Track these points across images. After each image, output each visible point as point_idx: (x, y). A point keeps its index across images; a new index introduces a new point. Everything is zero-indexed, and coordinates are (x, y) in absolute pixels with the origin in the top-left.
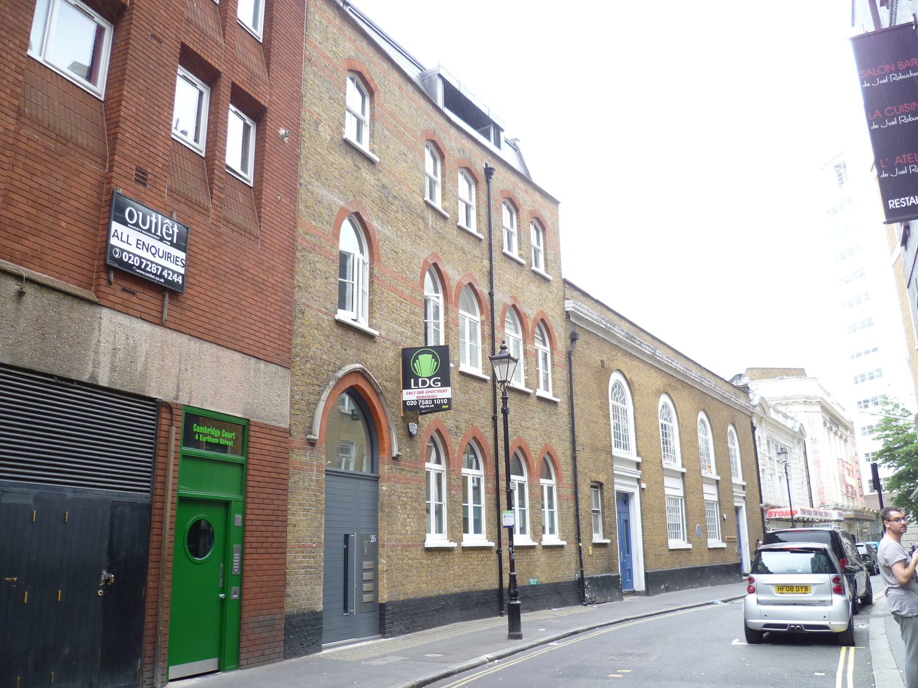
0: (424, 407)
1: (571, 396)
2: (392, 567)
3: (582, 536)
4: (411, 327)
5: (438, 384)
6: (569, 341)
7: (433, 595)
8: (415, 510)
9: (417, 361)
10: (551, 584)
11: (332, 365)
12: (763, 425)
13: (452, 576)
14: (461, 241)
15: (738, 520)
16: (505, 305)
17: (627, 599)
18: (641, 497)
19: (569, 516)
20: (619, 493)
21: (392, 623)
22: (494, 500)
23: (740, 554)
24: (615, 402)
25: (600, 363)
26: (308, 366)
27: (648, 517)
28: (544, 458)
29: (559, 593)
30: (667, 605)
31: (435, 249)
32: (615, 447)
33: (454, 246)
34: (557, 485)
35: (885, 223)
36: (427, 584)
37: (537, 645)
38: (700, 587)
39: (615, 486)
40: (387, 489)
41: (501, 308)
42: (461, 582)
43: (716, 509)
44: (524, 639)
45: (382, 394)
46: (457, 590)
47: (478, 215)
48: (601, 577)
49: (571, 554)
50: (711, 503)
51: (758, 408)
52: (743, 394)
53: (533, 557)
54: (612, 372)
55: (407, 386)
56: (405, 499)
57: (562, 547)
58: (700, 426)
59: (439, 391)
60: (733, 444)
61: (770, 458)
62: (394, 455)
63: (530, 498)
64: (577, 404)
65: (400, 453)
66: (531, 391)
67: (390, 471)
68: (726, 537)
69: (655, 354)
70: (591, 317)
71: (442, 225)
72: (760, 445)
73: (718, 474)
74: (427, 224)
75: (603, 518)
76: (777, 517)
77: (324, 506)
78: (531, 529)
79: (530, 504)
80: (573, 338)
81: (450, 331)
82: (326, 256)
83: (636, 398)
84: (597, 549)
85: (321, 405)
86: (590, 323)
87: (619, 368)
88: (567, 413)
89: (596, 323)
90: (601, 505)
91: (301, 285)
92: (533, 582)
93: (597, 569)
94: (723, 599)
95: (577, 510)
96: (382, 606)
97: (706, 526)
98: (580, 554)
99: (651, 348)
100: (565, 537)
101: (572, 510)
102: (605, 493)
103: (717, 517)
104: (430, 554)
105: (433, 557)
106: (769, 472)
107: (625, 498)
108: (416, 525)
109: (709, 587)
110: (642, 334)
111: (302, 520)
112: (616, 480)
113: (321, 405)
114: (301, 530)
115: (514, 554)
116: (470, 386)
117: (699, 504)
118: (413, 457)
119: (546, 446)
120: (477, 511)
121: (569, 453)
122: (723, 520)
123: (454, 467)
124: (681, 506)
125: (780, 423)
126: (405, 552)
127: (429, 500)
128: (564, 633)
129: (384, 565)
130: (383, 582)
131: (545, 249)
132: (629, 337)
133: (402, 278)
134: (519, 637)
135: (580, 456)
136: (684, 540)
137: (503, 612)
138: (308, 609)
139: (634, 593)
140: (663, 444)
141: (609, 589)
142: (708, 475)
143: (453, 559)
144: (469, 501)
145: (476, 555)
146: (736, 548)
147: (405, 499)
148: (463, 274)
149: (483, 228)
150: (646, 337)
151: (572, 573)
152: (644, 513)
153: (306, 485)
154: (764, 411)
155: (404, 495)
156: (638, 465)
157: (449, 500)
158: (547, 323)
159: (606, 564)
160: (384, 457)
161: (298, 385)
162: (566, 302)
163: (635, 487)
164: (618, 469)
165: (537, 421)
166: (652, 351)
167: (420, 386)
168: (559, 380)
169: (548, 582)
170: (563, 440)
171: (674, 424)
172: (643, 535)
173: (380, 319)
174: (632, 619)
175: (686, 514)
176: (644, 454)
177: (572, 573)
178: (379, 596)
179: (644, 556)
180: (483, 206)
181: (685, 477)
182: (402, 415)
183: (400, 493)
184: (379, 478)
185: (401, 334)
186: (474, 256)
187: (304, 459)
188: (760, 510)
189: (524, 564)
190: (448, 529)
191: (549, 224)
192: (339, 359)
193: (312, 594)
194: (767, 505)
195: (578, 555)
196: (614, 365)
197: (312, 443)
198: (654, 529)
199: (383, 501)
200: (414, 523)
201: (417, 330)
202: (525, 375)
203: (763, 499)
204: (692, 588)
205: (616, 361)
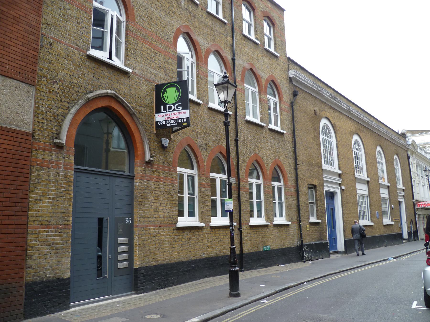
0: (170, 125)
1: (294, 130)
2: (145, 242)
3: (302, 219)
4: (165, 72)
5: (179, 108)
6: (292, 96)
7: (184, 260)
8: (167, 201)
9: (165, 93)
10: (279, 249)
11: (83, 88)
12: (414, 156)
13: (202, 247)
14: (210, 22)
15: (400, 209)
16: (244, 69)
17: (333, 256)
18: (341, 195)
19: (293, 206)
20: (327, 192)
21: (144, 282)
22: (236, 195)
23: (401, 228)
24: (324, 137)
25: (313, 112)
26: (56, 86)
27: (346, 207)
28: (275, 168)
29: (286, 255)
30: (357, 261)
31: (187, 23)
32: (325, 164)
33: (204, 24)
34: (284, 186)
36: (179, 253)
37: (250, 303)
38: (378, 247)
39: (325, 188)
40: (140, 184)
41: (241, 70)
42: (210, 250)
43: (388, 202)
44: (241, 296)
45: (135, 115)
46: (206, 256)
47: (223, 8)
48: (315, 244)
49: (294, 230)
50: (385, 199)
51: (411, 146)
52: (402, 138)
53: (267, 232)
54: (322, 118)
55: (158, 111)
56: (159, 192)
57: (288, 225)
58: (378, 156)
59: (180, 113)
60: (397, 166)
61: (418, 175)
62: (147, 160)
63: (264, 194)
64: (298, 135)
65: (152, 159)
66: (264, 125)
67: (143, 172)
68: (394, 218)
69: (350, 110)
70: (306, 82)
71: (193, 8)
72: (412, 167)
73: (388, 182)
74: (180, 5)
75: (317, 207)
76: (423, 207)
77: (72, 196)
78: (265, 214)
79: (264, 198)
80: (295, 94)
81: (200, 79)
82: (78, 7)
83: (338, 135)
84: (313, 227)
85: (69, 118)
86: (307, 86)
87: (327, 116)
88: (291, 141)
89: (310, 86)
90: (316, 199)
91: (49, 23)
92: (266, 248)
94: (394, 256)
95: (298, 202)
96: (136, 270)
97: (382, 212)
98: (301, 230)
99: (347, 106)
100: (290, 219)
101: (295, 202)
102: (318, 192)
103: (388, 206)
104: (181, 231)
105: (185, 234)
106: (418, 182)
107: (331, 195)
108: (168, 211)
109: (384, 248)
110: (341, 98)
111: (46, 207)
112: (325, 184)
113: (69, 118)
114: (45, 214)
115: (234, 232)
116: (217, 118)
117: (378, 199)
118: (166, 163)
119: (276, 161)
120: (259, 204)
121: (292, 166)
122: (392, 209)
123: (204, 171)
124: (367, 201)
125: (423, 155)
126: (158, 231)
127: (275, 201)
128: (277, 290)
129: (137, 240)
130: (137, 253)
131: (274, 38)
132: (332, 97)
133: (157, 36)
134: (238, 295)
136: (369, 220)
137: (243, 269)
138: (53, 277)
139: (338, 252)
140: (356, 163)
141: (320, 251)
142: (383, 183)
143: (202, 234)
144: (276, 200)
145: (222, 232)
146: (399, 224)
147: (159, 192)
148: (211, 44)
149: (228, 16)
150: (344, 99)
151: (295, 242)
152: (343, 204)
153: (52, 178)
154: (415, 148)
155: (157, 189)
156: (340, 175)
157: (200, 194)
158: (276, 83)
160: (138, 161)
161: (44, 100)
162: (290, 71)
163: (338, 188)
164: (326, 177)
165: (269, 144)
166: (348, 107)
167: (167, 110)
168: (285, 120)
169: (277, 248)
170: (289, 157)
171: (363, 152)
172: (343, 217)
173: (134, 62)
174: (333, 274)
175: (370, 205)
176: (343, 169)
177: (295, 242)
178: (134, 263)
179: (344, 230)
180: (227, 2)
181: (369, 184)
182: (155, 132)
183: (153, 188)
184: (134, 176)
185: (156, 75)
186: (220, 33)
187: (50, 158)
188: (412, 203)
189: (260, 237)
190: (199, 214)
191: (277, 22)
192: (91, 85)
193: (58, 265)
194: (417, 201)
195: (299, 230)
196: (323, 114)
197: (60, 147)
198: (350, 214)
199: (136, 194)
200: (167, 209)
201: (171, 75)
202: (260, 115)
203: (415, 197)
204: (374, 248)
205: (324, 112)
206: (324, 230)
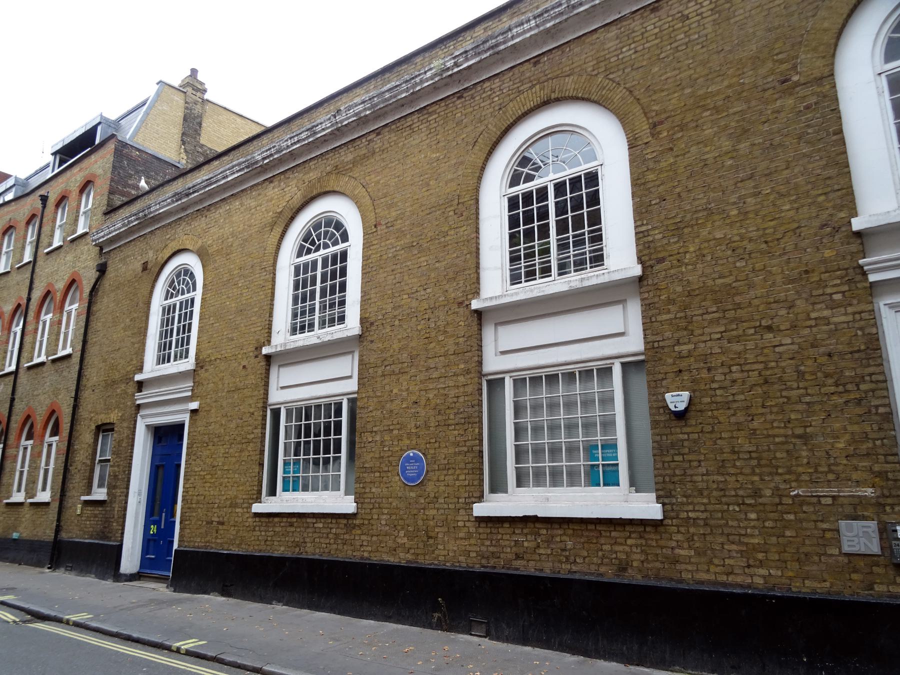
35: (101, 115)
84: (89, 508)
92: (15, 535)
93: (85, 533)
119: (52, 404)
135: (86, 394)
159: (99, 528)
206: (113, 517)
